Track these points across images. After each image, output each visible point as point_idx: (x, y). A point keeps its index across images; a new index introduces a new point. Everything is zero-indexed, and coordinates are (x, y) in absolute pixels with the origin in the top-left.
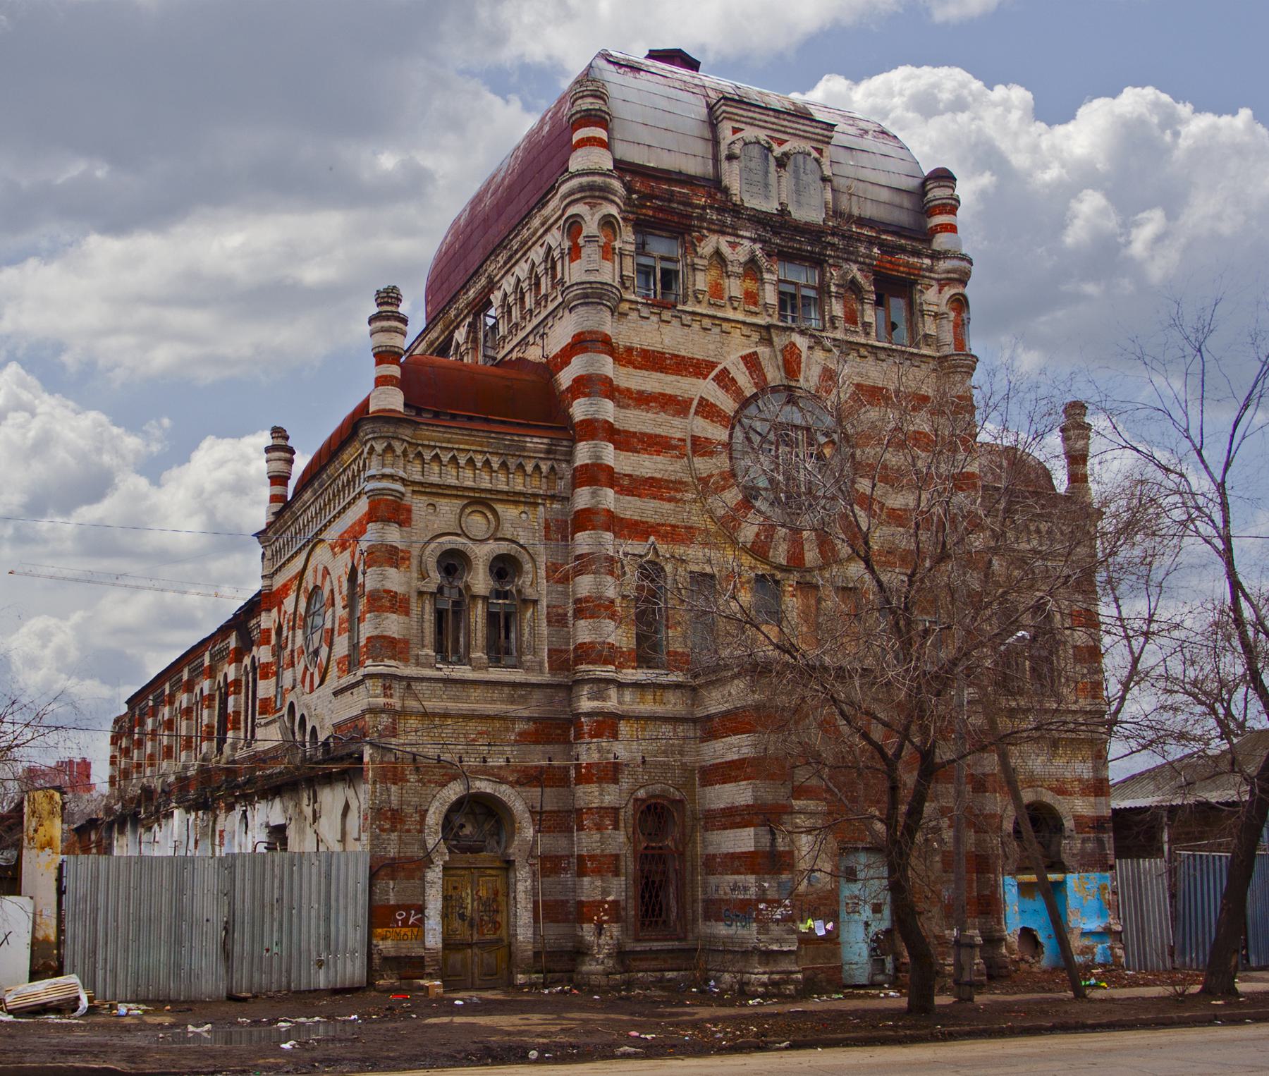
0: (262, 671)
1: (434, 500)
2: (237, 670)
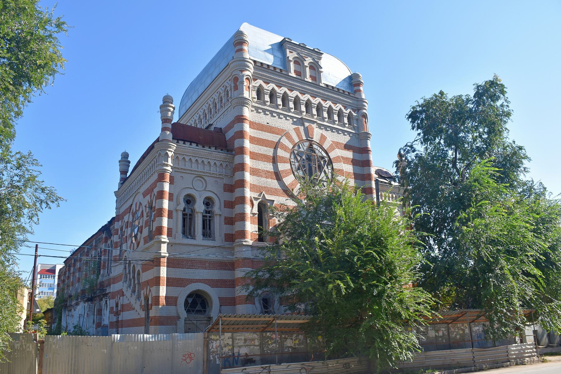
0: (116, 245)
1: (183, 175)
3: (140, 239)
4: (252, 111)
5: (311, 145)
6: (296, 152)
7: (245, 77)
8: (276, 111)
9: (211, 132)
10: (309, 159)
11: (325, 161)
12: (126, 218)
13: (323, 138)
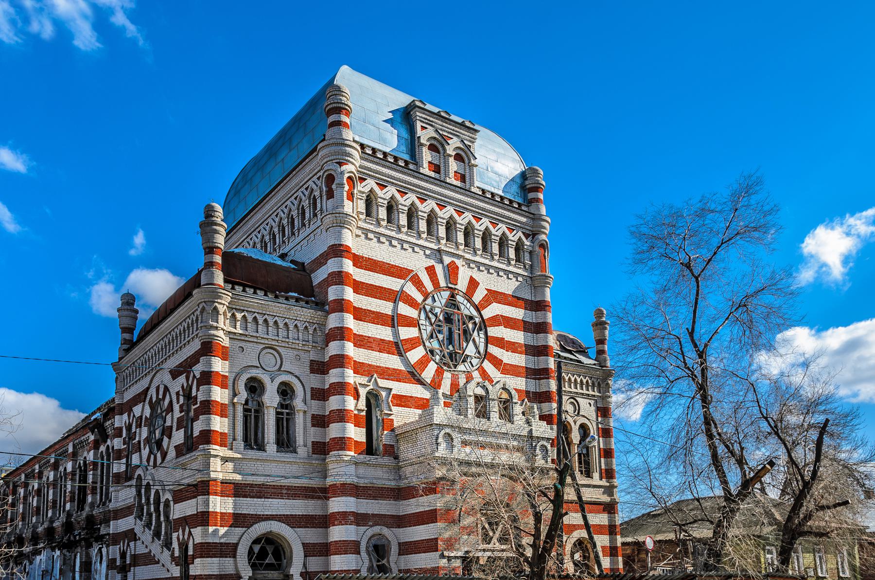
0: (119, 455)
1: (242, 344)
2: (95, 455)
3: (168, 448)
4: (357, 236)
5: (453, 296)
6: (428, 308)
7: (347, 175)
8: (397, 236)
10: (448, 319)
11: (475, 324)
12: (137, 410)
13: (473, 284)
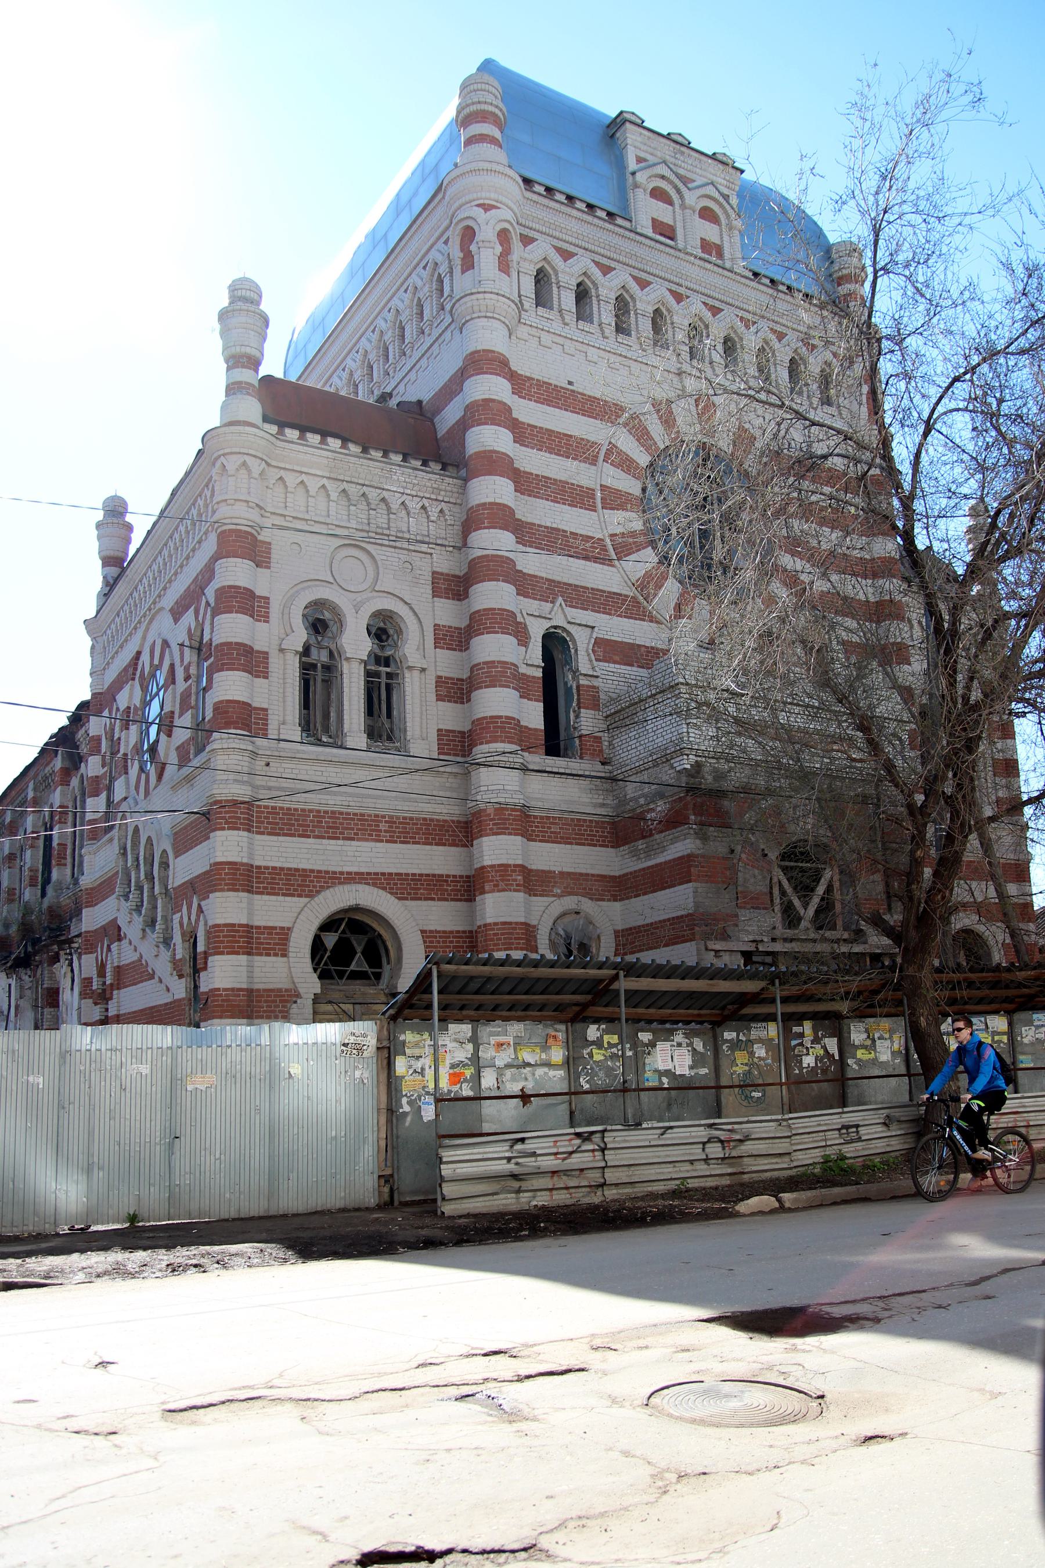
0: (95, 787)
3: (167, 755)
9: (390, 411)
12: (123, 700)
